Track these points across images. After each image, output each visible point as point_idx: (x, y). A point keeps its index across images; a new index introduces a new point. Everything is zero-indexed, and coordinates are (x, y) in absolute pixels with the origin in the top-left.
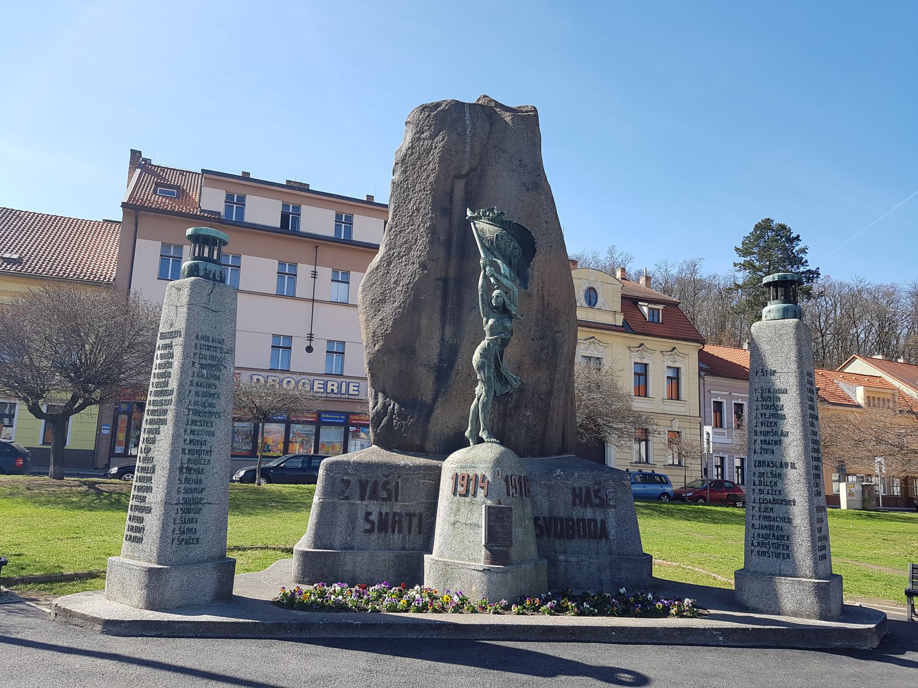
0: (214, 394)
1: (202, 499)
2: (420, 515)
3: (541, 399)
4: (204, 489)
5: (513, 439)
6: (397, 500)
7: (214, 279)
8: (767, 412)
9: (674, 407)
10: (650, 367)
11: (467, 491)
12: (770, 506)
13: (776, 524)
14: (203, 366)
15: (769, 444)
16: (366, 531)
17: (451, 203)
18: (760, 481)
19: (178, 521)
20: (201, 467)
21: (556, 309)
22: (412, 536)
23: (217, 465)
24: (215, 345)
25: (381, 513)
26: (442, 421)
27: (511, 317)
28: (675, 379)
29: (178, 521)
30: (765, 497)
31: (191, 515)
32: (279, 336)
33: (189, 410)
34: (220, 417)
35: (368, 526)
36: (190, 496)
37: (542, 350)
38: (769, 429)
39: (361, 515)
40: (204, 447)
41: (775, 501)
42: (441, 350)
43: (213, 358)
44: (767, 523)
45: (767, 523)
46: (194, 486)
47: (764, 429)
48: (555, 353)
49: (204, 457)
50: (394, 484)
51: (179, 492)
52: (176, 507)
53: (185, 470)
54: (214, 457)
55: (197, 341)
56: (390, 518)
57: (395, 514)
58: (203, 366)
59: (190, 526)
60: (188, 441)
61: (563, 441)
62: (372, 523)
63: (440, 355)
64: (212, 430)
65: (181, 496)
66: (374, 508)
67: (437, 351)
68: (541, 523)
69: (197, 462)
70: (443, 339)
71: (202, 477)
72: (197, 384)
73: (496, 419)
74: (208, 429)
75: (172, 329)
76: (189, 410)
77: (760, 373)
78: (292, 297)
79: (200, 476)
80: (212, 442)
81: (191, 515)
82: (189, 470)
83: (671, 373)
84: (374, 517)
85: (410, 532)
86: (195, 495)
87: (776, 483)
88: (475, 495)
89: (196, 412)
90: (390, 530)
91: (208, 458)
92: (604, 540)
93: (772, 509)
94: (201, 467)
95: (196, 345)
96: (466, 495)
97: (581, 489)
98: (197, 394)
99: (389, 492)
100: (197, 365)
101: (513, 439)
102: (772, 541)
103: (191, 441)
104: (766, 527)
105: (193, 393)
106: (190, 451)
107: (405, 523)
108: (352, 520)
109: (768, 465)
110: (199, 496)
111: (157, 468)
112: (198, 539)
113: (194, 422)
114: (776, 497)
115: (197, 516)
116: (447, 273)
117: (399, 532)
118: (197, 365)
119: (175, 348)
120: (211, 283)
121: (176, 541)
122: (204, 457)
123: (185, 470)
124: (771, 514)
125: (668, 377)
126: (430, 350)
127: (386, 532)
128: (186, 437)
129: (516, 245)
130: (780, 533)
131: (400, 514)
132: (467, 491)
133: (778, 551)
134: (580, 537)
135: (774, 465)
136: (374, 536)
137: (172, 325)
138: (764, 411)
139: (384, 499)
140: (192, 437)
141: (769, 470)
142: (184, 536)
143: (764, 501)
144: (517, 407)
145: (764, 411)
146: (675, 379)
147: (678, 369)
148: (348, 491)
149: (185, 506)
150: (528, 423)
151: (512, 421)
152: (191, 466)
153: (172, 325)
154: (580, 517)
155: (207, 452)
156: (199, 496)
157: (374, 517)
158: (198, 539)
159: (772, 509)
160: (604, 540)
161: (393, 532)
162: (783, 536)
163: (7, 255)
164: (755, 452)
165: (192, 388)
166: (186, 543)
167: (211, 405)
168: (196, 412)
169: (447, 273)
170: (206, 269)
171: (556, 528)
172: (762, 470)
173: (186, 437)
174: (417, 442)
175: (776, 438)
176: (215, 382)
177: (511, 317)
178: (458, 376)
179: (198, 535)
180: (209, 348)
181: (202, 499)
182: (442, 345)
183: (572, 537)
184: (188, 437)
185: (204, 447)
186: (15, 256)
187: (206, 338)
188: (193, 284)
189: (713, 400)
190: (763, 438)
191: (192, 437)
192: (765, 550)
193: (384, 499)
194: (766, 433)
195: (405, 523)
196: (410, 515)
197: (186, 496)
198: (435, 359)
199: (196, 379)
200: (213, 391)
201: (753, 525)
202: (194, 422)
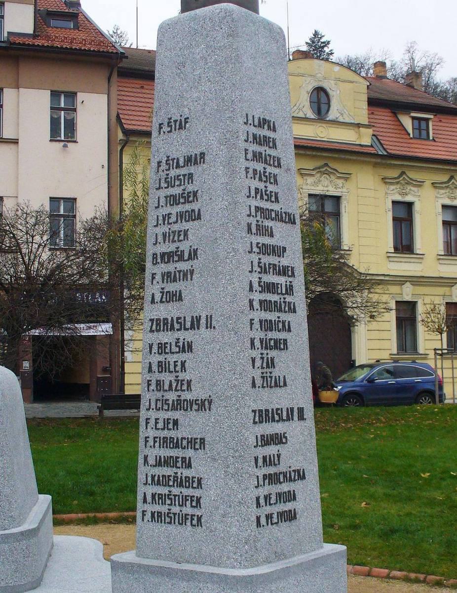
8: (175, 210)
10: (417, 207)
29: (258, 363)
38: (172, 247)
41: (178, 405)
93: (176, 423)
109: (172, 328)
135: (183, 327)
201: (146, 458)
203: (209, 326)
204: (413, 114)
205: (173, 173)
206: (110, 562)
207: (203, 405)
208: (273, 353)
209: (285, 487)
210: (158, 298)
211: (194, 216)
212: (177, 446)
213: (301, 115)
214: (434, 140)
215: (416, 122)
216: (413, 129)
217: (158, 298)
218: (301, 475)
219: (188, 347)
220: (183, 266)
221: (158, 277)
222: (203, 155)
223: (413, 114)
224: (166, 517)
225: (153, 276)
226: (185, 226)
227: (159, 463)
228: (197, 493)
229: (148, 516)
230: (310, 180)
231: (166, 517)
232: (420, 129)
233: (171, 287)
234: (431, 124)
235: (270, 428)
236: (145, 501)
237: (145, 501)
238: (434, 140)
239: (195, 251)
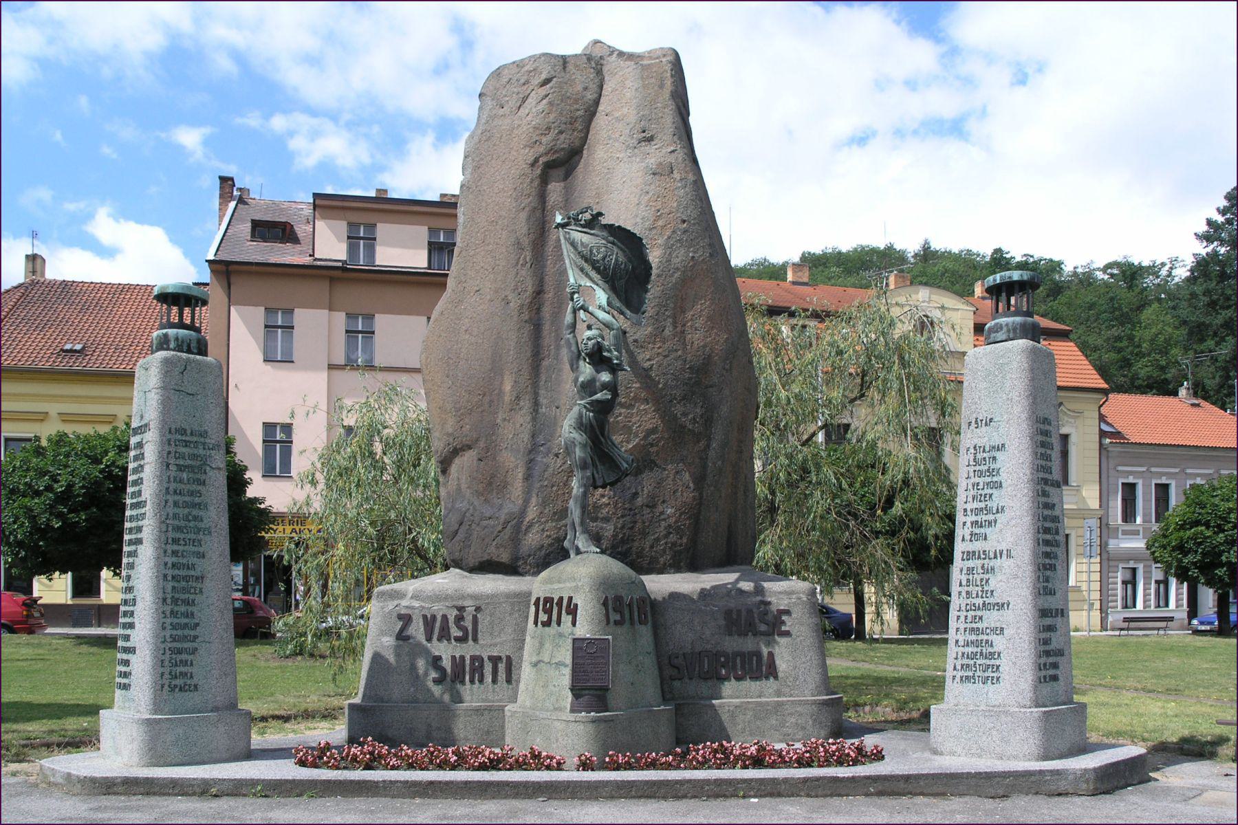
0: (200, 504)
4: (197, 625)
8: (981, 480)
12: (979, 613)
13: (985, 637)
14: (180, 468)
18: (968, 580)
19: (167, 663)
20: (192, 597)
24: (195, 439)
25: (453, 657)
29: (167, 663)
30: (974, 601)
31: (184, 657)
32: (273, 425)
38: (982, 505)
43: (194, 457)
44: (974, 637)
45: (974, 637)
47: (976, 505)
54: (208, 584)
56: (468, 662)
58: (180, 468)
60: (170, 565)
64: (201, 550)
69: (185, 590)
71: (194, 609)
72: (175, 492)
74: (196, 549)
78: (370, 367)
79: (190, 609)
80: (202, 566)
81: (184, 657)
86: (187, 632)
88: (559, 624)
91: (199, 585)
93: (981, 618)
96: (547, 624)
97: (739, 611)
98: (176, 504)
99: (465, 630)
102: (978, 662)
103: (173, 565)
106: (173, 577)
107: (488, 668)
109: (979, 558)
110: (192, 633)
111: (138, 599)
115: (191, 657)
119: (146, 447)
121: (166, 687)
124: (979, 625)
128: (167, 559)
130: (990, 650)
133: (986, 674)
137: (142, 417)
138: (977, 480)
139: (458, 639)
140: (174, 559)
141: (979, 562)
145: (977, 480)
152: (177, 596)
153: (142, 417)
155: (197, 578)
163: (68, 347)
166: (181, 690)
167: (196, 518)
168: (178, 529)
172: (971, 564)
176: (200, 488)
180: (187, 444)
181: (196, 637)
185: (192, 573)
186: (78, 347)
187: (183, 431)
188: (166, 362)
190: (974, 518)
192: (971, 674)
194: (977, 511)
195: (488, 668)
197: (175, 632)
200: (197, 500)
203: (1009, 556)
206: (414, 659)
207: (1001, 606)
208: (1048, 573)
220: (991, 517)
221: (968, 524)
222: (1003, 445)
224: (470, 628)
228: (997, 662)
231: (470, 628)
237: (955, 669)
239: (1003, 508)
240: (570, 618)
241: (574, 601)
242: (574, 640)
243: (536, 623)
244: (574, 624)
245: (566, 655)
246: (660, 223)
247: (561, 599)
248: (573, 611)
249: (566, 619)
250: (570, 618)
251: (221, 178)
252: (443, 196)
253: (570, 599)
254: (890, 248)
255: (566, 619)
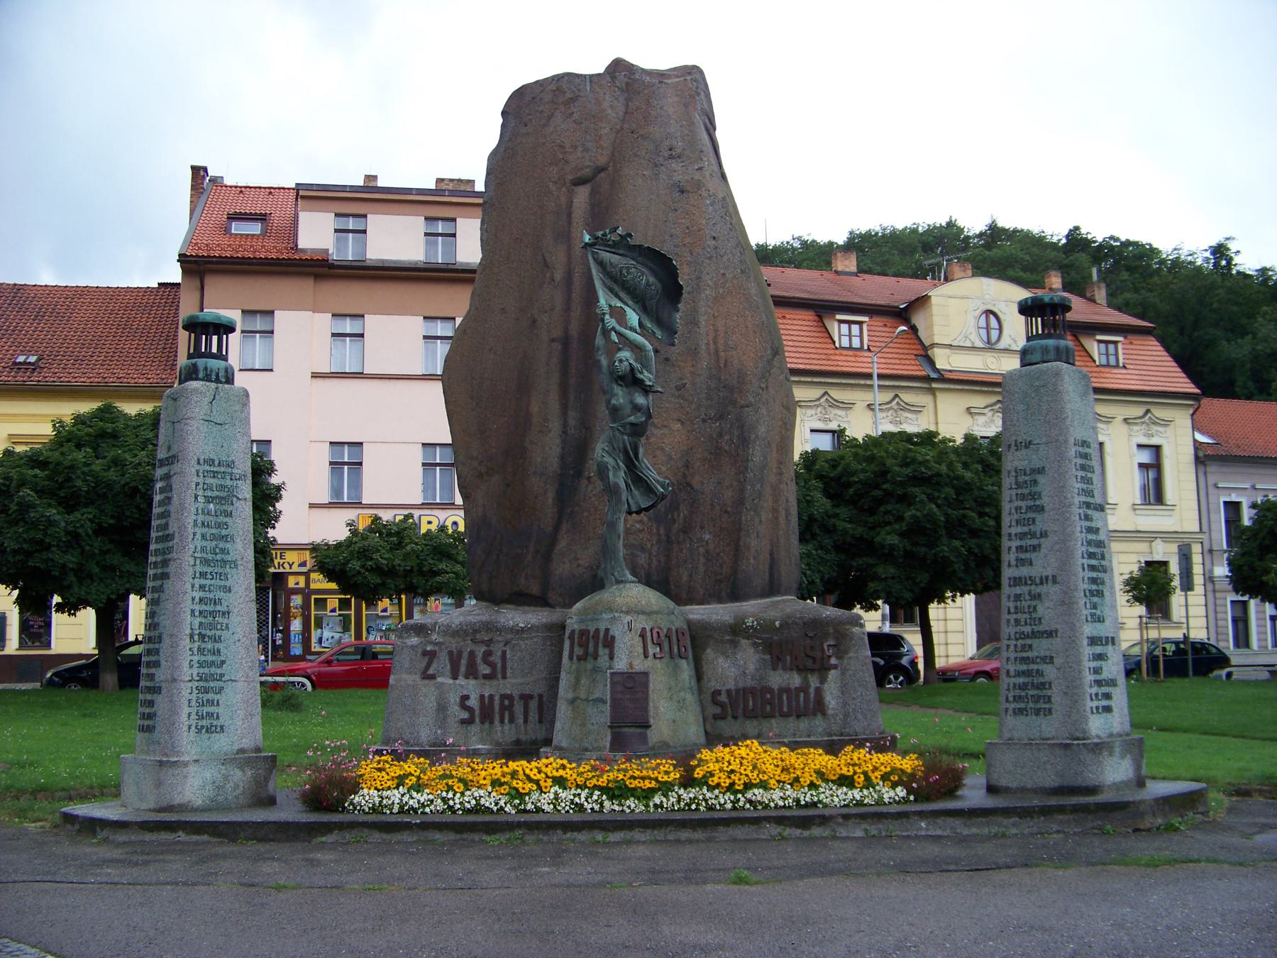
1: (222, 675)
2: (540, 696)
3: (726, 512)
4: (223, 662)
5: (685, 578)
6: (504, 677)
7: (218, 381)
8: (1023, 504)
9: (1153, 520)
11: (586, 653)
12: (1029, 642)
13: (1035, 667)
14: (209, 500)
15: (1026, 551)
16: (463, 722)
17: (570, 223)
18: (1016, 607)
19: (193, 703)
20: (218, 633)
21: (739, 370)
22: (530, 726)
23: (239, 630)
24: (222, 469)
25: (482, 697)
26: (570, 561)
27: (646, 390)
28: (1153, 468)
29: (193, 703)
33: (195, 558)
34: (236, 566)
35: (465, 715)
36: (206, 670)
37: (721, 435)
38: (1026, 529)
39: (454, 699)
40: (218, 608)
41: (1034, 635)
42: (563, 448)
43: (222, 487)
45: (1024, 667)
46: (210, 658)
47: (1020, 529)
48: (744, 442)
49: (221, 620)
50: (499, 653)
51: (191, 667)
52: (190, 684)
53: (196, 637)
54: (234, 619)
55: (198, 467)
57: (503, 697)
58: (209, 500)
59: (211, 709)
60: (197, 600)
61: (771, 575)
62: (470, 710)
63: (562, 458)
64: (228, 584)
65: (195, 671)
66: (472, 688)
67: (556, 451)
68: (723, 698)
69: (212, 626)
70: (565, 432)
71: (221, 646)
73: (655, 548)
74: (223, 583)
75: (170, 454)
76: (195, 558)
77: (1013, 448)
79: (217, 646)
80: (230, 600)
81: (210, 696)
82: (202, 636)
83: (1145, 457)
84: (473, 702)
85: (526, 721)
86: (213, 670)
87: (1035, 608)
89: (206, 562)
90: (497, 722)
91: (226, 621)
92: (819, 717)
93: (1030, 646)
94: (218, 633)
95: (198, 472)
98: (203, 537)
100: (201, 499)
101: (685, 578)
102: (1031, 693)
103: (201, 600)
104: (1023, 672)
105: (198, 536)
106: (201, 612)
107: (518, 708)
108: (442, 708)
109: (1026, 584)
110: (219, 671)
111: (164, 636)
112: (222, 727)
113: (203, 575)
114: (1036, 628)
115: (218, 696)
116: (566, 330)
117: (512, 720)
118: (201, 499)
120: (213, 385)
122: (221, 620)
123: (196, 637)
124: (1030, 654)
125: (1141, 465)
126: (547, 450)
127: (492, 723)
128: (195, 594)
129: (652, 279)
130: (1041, 680)
131: (510, 697)
132: (586, 653)
133: (1038, 706)
134: (783, 715)
136: (475, 728)
138: (1020, 503)
139: (486, 677)
140: (202, 594)
141: (1026, 589)
142: (204, 723)
143: (1023, 636)
144: (685, 530)
146: (1153, 468)
147: (1157, 449)
148: (434, 665)
149: (201, 684)
150: (707, 552)
151: (681, 550)
152: (203, 632)
154: (784, 685)
155: (224, 613)
156: (219, 671)
157: (473, 702)
158: (222, 727)
159: (1030, 646)
160: (819, 717)
161: (502, 721)
162: (1043, 684)
164: (1009, 565)
165: (197, 529)
167: (223, 551)
168: (206, 562)
169: (566, 330)
170: (206, 369)
171: (746, 705)
172: (1018, 590)
173: (195, 594)
174: (535, 589)
175: (1035, 542)
177: (646, 390)
178: (590, 487)
179: (221, 722)
180: (215, 475)
181: (222, 675)
182: (564, 442)
183: (772, 716)
184: (198, 595)
185: (218, 608)
187: (210, 462)
189: (1222, 499)
190: (1018, 543)
191: (202, 594)
193: (486, 677)
195: (518, 708)
196: (526, 698)
197: (202, 670)
198: (554, 464)
199: (201, 518)
200: (224, 532)
201: (1008, 672)
202: (203, 575)
204: (1099, 337)
205: (1021, 479)
207: (1050, 634)
209: (1105, 689)
210: (1013, 563)
211: (1041, 509)
212: (1033, 662)
213: (968, 344)
214: (869, 349)
215: (1103, 346)
216: (1100, 354)
217: (1013, 563)
218: (1112, 683)
219: (1038, 597)
221: (1014, 549)
223: (1099, 337)
225: (1010, 548)
226: (1032, 515)
227: (1018, 674)
229: (1010, 712)
230: (981, 419)
232: (1107, 354)
233: (1022, 556)
234: (1120, 346)
235: (1098, 649)
236: (1007, 700)
238: (1124, 367)
240: (607, 651)
241: (611, 633)
242: (612, 674)
243: (571, 658)
244: (611, 658)
245: (604, 690)
246: (688, 240)
247: (597, 631)
248: (610, 643)
249: (603, 652)
250: (607, 651)
251: (193, 168)
252: (439, 181)
253: (607, 630)
254: (503, 113)
255: (603, 652)
